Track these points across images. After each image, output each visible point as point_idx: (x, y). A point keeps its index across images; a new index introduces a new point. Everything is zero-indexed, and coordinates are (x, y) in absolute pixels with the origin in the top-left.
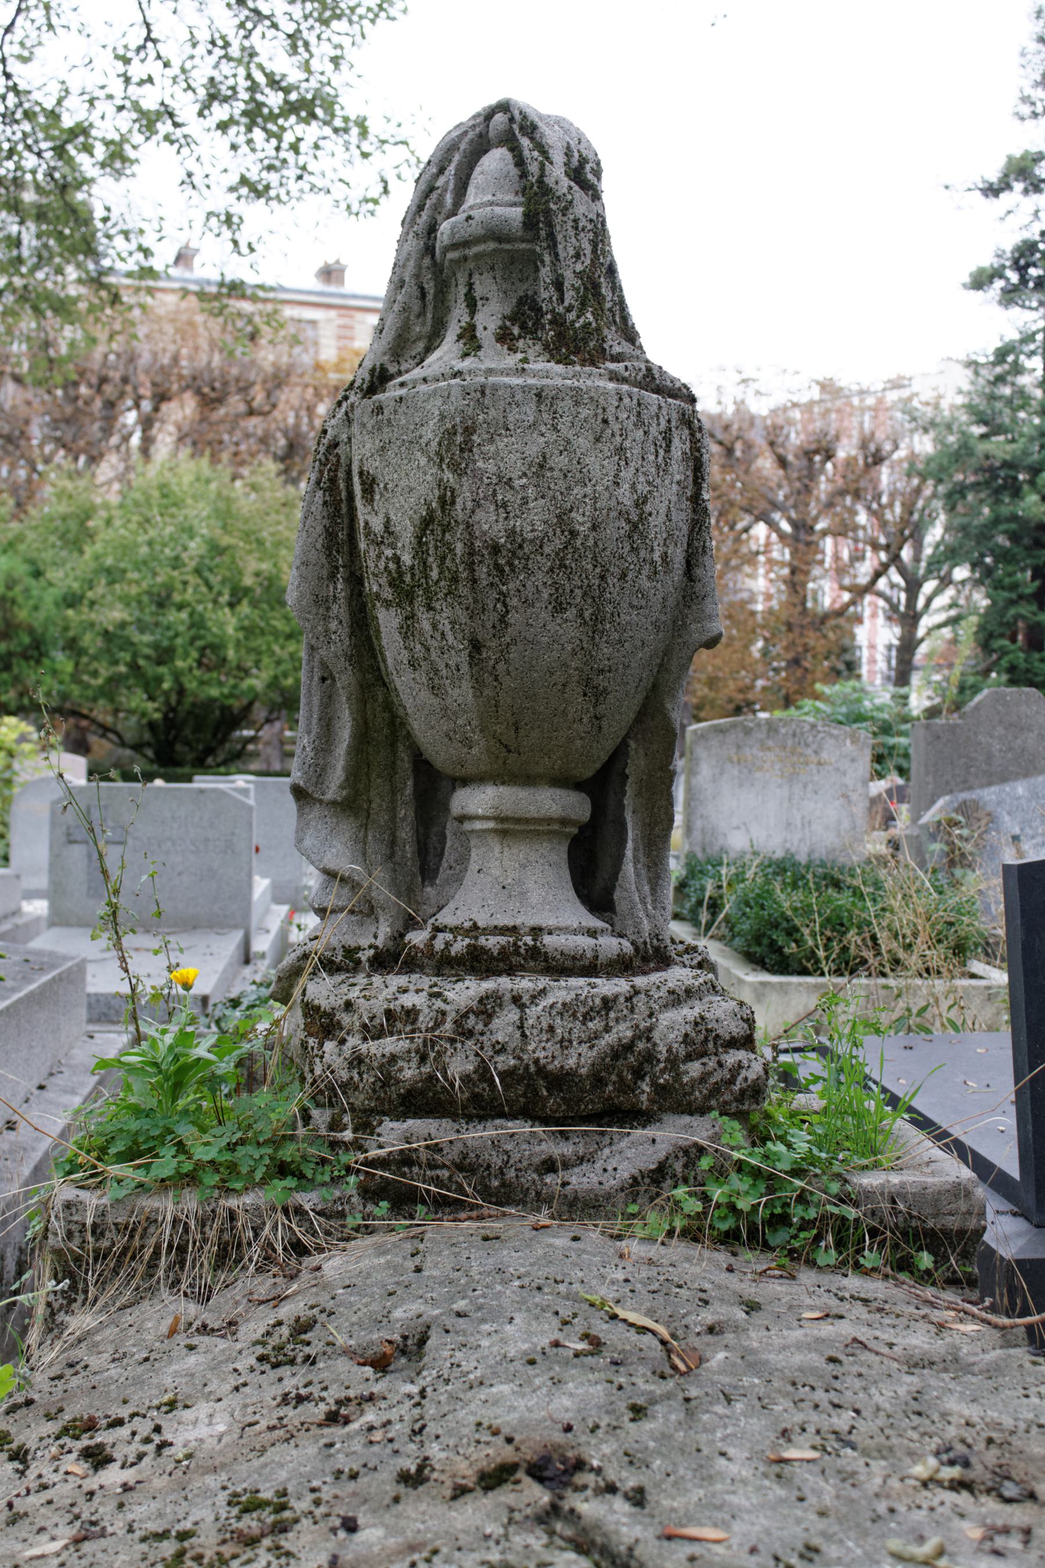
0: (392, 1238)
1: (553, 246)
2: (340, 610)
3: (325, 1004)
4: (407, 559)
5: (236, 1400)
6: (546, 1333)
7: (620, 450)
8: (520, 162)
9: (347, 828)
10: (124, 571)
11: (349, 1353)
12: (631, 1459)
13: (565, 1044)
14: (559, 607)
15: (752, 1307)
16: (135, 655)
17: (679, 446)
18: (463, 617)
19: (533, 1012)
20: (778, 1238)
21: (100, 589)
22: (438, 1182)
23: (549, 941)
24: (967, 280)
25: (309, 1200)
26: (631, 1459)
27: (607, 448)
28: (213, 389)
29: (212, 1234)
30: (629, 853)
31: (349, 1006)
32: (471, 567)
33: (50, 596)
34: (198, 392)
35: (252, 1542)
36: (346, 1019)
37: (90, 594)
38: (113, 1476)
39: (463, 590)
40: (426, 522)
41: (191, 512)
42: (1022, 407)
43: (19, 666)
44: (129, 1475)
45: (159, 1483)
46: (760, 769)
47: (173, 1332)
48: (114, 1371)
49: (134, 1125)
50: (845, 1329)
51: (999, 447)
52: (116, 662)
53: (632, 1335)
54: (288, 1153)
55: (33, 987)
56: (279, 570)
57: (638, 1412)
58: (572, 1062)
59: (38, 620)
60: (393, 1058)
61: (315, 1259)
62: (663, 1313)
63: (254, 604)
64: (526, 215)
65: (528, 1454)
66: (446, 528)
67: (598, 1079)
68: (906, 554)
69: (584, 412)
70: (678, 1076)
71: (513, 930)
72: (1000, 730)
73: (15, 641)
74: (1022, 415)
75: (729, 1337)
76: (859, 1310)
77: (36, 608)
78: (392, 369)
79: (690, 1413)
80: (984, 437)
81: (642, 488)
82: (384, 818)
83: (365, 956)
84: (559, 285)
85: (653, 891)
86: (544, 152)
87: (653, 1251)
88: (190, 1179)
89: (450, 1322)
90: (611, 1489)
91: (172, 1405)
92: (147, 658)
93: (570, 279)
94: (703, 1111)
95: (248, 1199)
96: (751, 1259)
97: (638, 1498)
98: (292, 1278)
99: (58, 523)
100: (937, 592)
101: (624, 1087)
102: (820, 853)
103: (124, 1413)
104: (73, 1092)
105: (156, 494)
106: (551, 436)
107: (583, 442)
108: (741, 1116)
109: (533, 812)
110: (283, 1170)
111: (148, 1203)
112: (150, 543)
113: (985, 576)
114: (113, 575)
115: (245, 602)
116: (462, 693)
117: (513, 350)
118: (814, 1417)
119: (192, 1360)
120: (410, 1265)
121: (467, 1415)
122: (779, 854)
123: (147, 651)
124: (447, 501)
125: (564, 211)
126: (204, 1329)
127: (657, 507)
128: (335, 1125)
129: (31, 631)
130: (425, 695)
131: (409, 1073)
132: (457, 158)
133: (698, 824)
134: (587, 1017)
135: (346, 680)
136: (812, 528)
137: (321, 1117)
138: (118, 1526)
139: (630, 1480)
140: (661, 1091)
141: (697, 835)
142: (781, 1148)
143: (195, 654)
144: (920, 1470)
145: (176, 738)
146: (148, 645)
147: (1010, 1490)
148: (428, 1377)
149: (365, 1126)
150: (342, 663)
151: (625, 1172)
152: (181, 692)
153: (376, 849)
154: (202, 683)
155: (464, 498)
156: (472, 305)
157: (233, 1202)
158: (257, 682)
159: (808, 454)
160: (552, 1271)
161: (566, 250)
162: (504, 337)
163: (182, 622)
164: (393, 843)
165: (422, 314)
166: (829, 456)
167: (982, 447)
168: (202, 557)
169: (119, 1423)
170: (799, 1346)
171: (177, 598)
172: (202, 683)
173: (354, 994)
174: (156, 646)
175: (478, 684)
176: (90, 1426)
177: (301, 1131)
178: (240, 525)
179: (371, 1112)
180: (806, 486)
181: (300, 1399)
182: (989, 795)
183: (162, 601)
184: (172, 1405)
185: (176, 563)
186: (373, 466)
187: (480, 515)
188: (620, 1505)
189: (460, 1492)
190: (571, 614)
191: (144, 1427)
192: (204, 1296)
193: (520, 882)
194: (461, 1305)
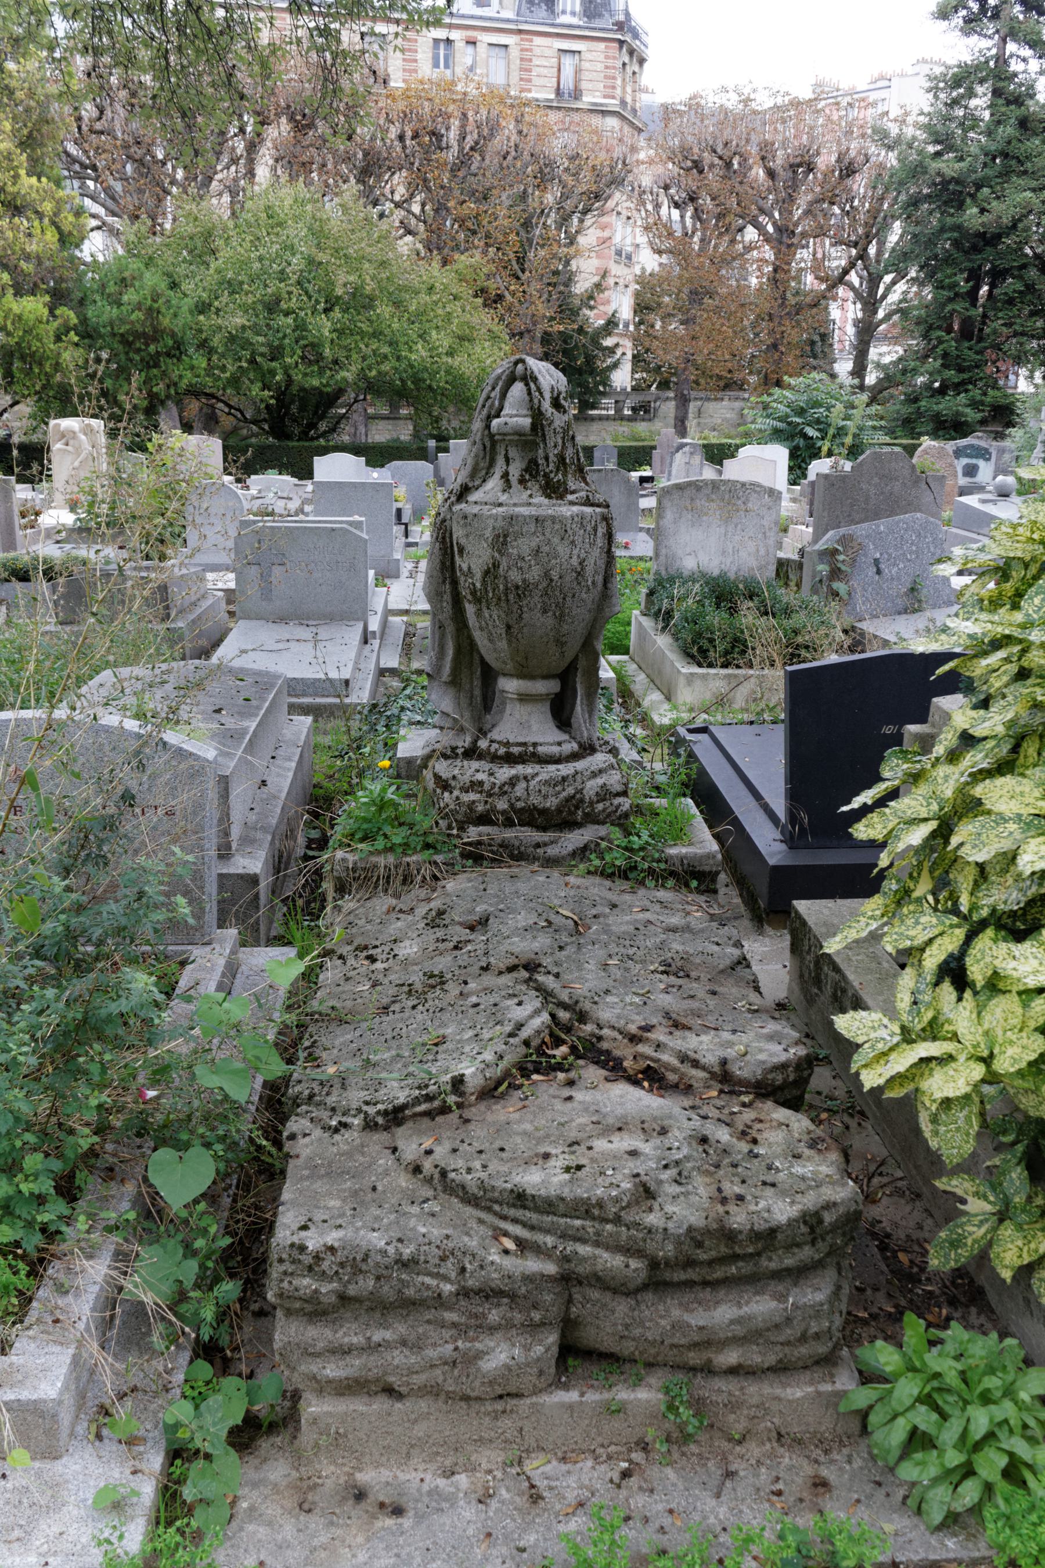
0: (474, 875)
1: (544, 440)
2: (447, 597)
3: (444, 776)
4: (478, 585)
5: (419, 940)
6: (532, 918)
7: (573, 542)
8: (529, 393)
9: (451, 691)
10: (241, 283)
11: (460, 924)
12: (556, 964)
13: (545, 797)
14: (545, 611)
15: (614, 906)
16: (253, 353)
17: (601, 530)
18: (503, 616)
19: (533, 783)
20: (631, 875)
21: (225, 298)
22: (492, 852)
23: (540, 749)
24: (934, 8)
25: (439, 858)
26: (556, 964)
27: (566, 542)
28: (304, 115)
29: (400, 872)
30: (578, 702)
31: (454, 777)
32: (506, 595)
33: (188, 303)
34: (292, 119)
35: (434, 987)
36: (453, 783)
37: (216, 303)
38: (379, 965)
39: (503, 604)
40: (487, 573)
41: (292, 232)
42: (972, 128)
43: (166, 363)
44: (385, 965)
45: (397, 968)
46: (706, 514)
47: (388, 912)
48: (369, 927)
49: (365, 826)
50: (648, 915)
51: (949, 166)
52: (240, 359)
53: (564, 920)
54: (430, 839)
55: (267, 704)
56: (363, 281)
57: (561, 948)
58: (548, 805)
59: (178, 325)
60: (474, 802)
61: (443, 883)
62: (577, 911)
63: (345, 311)
64: (532, 424)
65: (523, 962)
66: (496, 577)
67: (559, 811)
68: (872, 250)
69: (557, 527)
70: (593, 810)
71: (524, 744)
72: (876, 480)
73: (161, 343)
74: (971, 135)
75: (601, 919)
76: (657, 907)
77: (175, 315)
78: (470, 485)
79: (579, 949)
80: (938, 154)
81: (583, 555)
82: (467, 687)
83: (460, 751)
84: (547, 458)
85: (590, 716)
86: (541, 394)
87: (579, 881)
88: (391, 849)
89: (498, 913)
90: (549, 973)
91: (395, 941)
92: (262, 355)
93: (552, 458)
94: (603, 823)
95: (414, 858)
96: (621, 884)
97: (557, 975)
98: (434, 891)
99: (188, 241)
100: (894, 283)
101: (571, 813)
102: (744, 572)
103: (378, 943)
104: (290, 760)
105: (264, 215)
106: (542, 538)
107: (556, 540)
108: (619, 825)
109: (534, 692)
110: (427, 846)
111: (374, 859)
112: (261, 259)
113: (930, 273)
114: (234, 287)
115: (337, 309)
116: (503, 644)
117: (526, 488)
118: (622, 950)
119: (399, 924)
120: (482, 887)
121: (502, 948)
122: (716, 573)
123: (263, 349)
124: (496, 565)
125: (550, 425)
126: (401, 911)
127: (590, 563)
128: (450, 827)
129: (173, 335)
130: (486, 642)
131: (480, 808)
132: (500, 384)
133: (663, 551)
134: (555, 785)
135: (450, 628)
136: (793, 232)
137: (443, 824)
138: (386, 981)
139: (555, 970)
140: (586, 815)
141: (662, 558)
142: (636, 838)
143: (299, 352)
144: (652, 968)
145: (286, 414)
146: (263, 345)
147: (681, 974)
148: (490, 934)
149: (462, 829)
150: (449, 621)
151: (570, 848)
152: (289, 381)
153: (465, 702)
154: (305, 375)
155: (504, 565)
156: (507, 461)
157: (408, 859)
158: (348, 375)
159: (793, 167)
160: (536, 892)
161: (550, 443)
162: (522, 481)
163: (288, 327)
164: (472, 697)
165: (484, 457)
166: (810, 168)
167: (935, 165)
168: (301, 271)
169: (376, 947)
170: (627, 923)
171: (284, 305)
172: (305, 375)
173: (456, 772)
174: (270, 345)
175: (509, 642)
176: (366, 948)
177: (435, 830)
178: (331, 243)
179: (463, 822)
180: (790, 196)
181: (443, 940)
182: (861, 530)
183: (272, 306)
184: (395, 941)
185: (282, 276)
186: (463, 541)
187: (510, 573)
188: (551, 977)
189: (500, 973)
190: (550, 614)
191: (387, 949)
192: (397, 896)
193: (528, 721)
194: (501, 906)
